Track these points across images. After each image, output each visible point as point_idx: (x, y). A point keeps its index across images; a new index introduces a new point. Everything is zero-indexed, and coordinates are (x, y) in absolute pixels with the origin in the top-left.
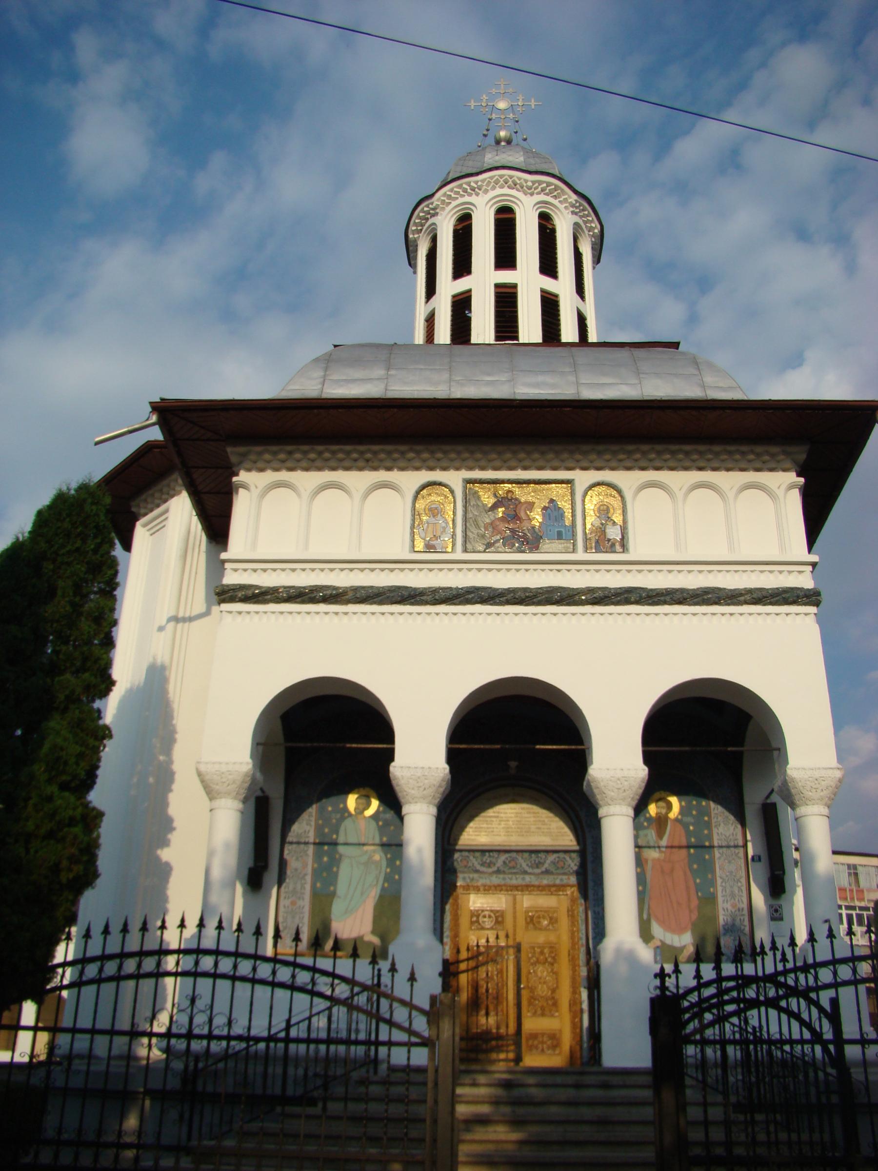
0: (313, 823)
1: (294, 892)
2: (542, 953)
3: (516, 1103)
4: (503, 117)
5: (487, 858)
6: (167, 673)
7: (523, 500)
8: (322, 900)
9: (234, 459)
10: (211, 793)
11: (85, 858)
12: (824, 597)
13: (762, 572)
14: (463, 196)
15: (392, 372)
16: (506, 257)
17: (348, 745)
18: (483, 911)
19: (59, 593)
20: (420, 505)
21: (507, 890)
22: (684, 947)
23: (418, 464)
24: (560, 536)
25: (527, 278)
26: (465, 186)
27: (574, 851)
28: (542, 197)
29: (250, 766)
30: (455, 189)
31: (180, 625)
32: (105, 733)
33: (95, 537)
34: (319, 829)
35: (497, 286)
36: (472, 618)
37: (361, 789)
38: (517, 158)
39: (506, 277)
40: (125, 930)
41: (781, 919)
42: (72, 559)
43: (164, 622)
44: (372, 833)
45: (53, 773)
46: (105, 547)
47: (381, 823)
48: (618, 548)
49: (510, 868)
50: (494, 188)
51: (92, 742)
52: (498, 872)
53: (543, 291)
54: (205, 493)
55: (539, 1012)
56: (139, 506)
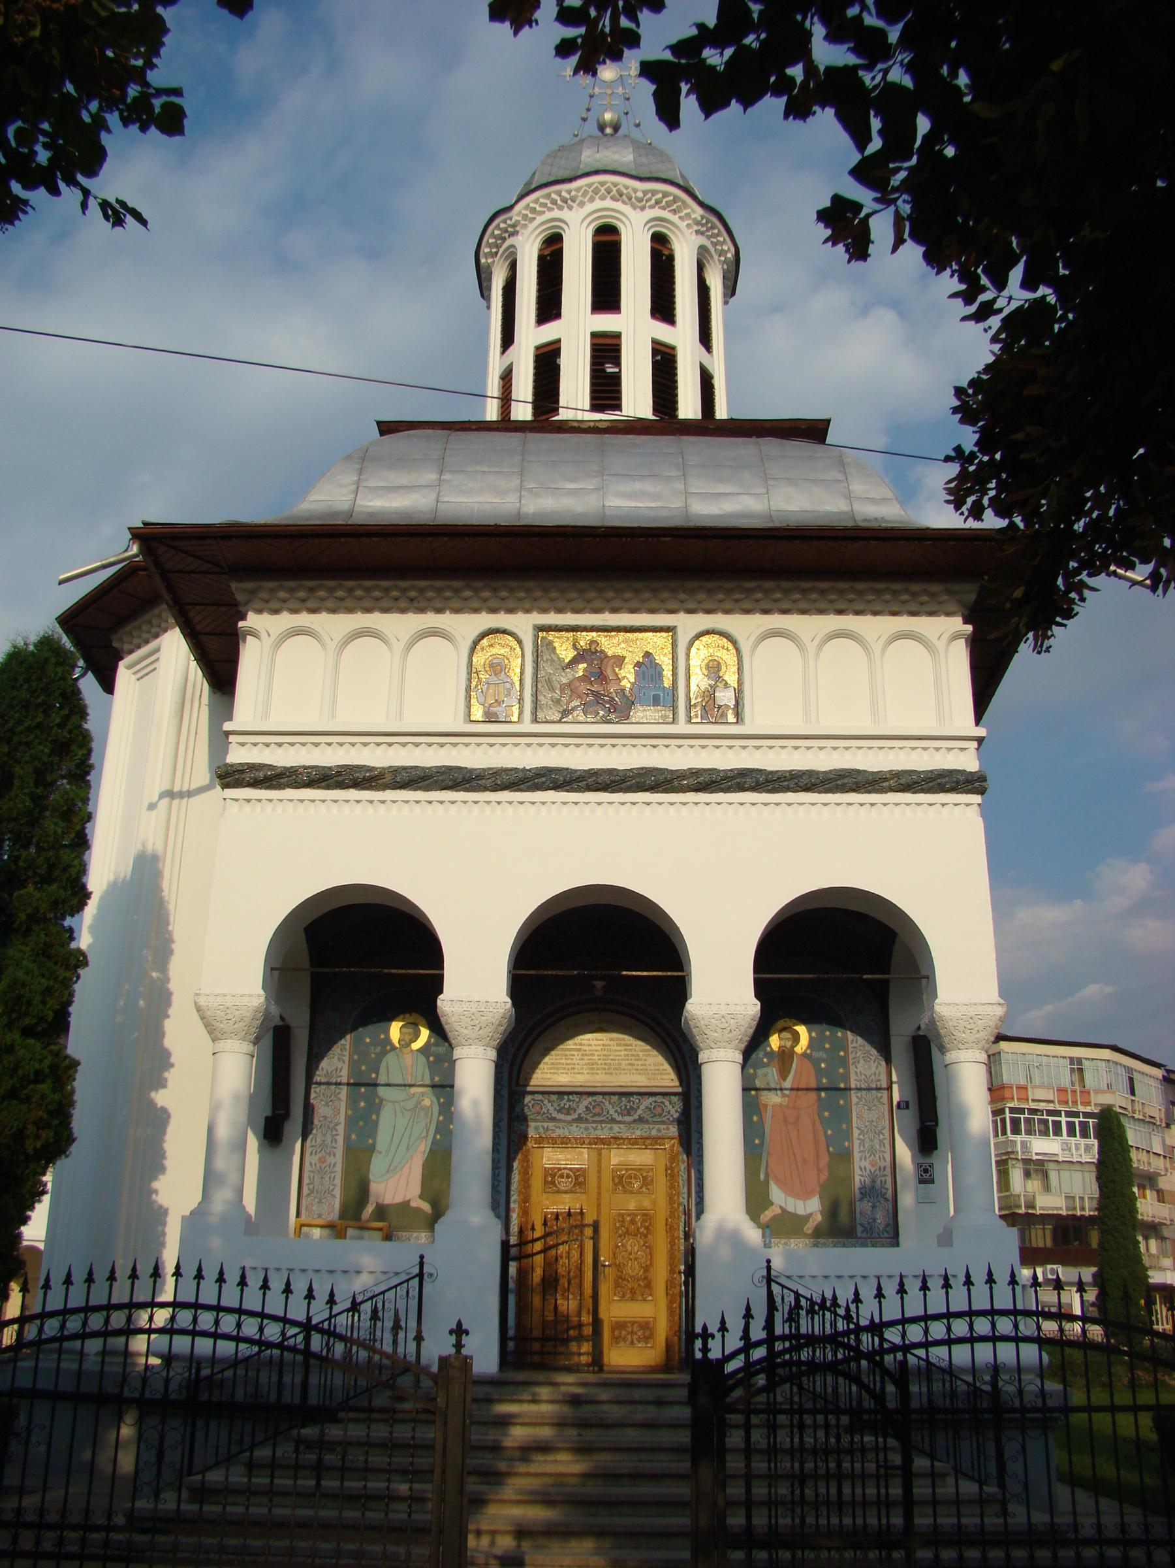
0: (346, 1059)
1: (323, 1145)
2: (633, 1222)
3: (583, 1424)
4: (609, 92)
5: (565, 1102)
6: (161, 865)
7: (610, 653)
8: (358, 1157)
9: (240, 597)
10: (214, 1033)
11: (56, 1122)
12: (990, 784)
13: (913, 749)
14: (551, 210)
15: (447, 477)
16: (606, 296)
17: (386, 971)
18: (560, 1169)
19: (17, 782)
20: (479, 659)
21: (590, 1144)
22: (811, 1214)
23: (476, 605)
24: (656, 701)
25: (635, 324)
26: (553, 196)
27: (675, 1094)
28: (657, 212)
29: (262, 999)
30: (542, 200)
31: (176, 802)
32: (79, 960)
33: (62, 707)
34: (353, 1066)
35: (594, 335)
36: (544, 808)
37: (407, 1015)
38: (624, 157)
39: (606, 322)
40: (90, 1279)
41: (932, 1181)
42: (32, 737)
43: (156, 798)
44: (420, 1071)
45: (14, 1016)
46: (75, 719)
47: (431, 1059)
48: (731, 718)
49: (595, 1115)
50: (592, 200)
51: (62, 973)
52: (579, 1120)
53: (655, 342)
54: (205, 634)
55: (628, 1296)
56: (121, 640)
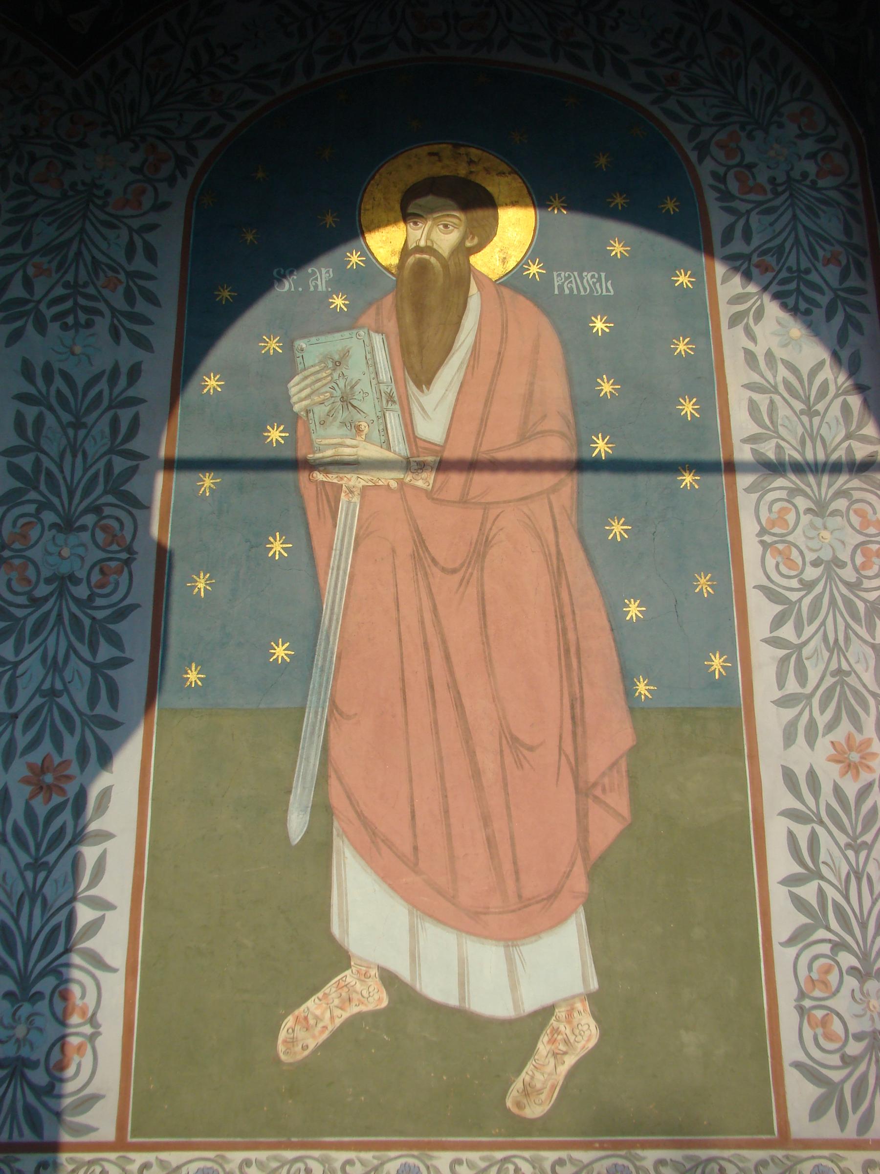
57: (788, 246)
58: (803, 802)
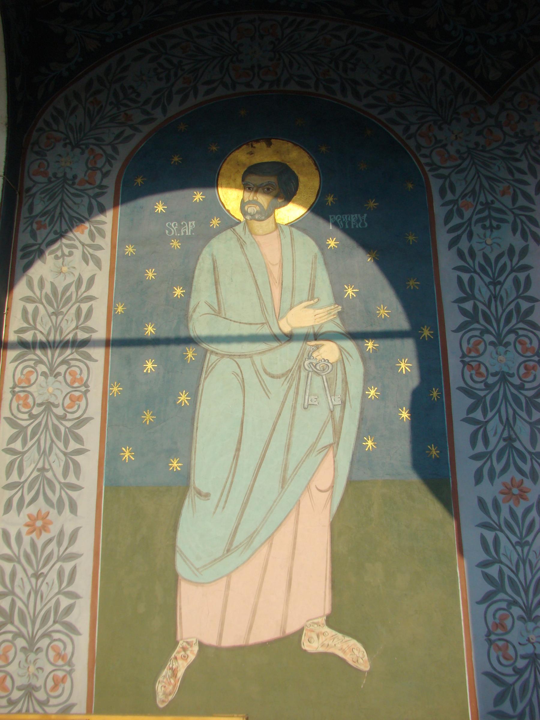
0: (105, 256)
57: (477, 188)
58: (490, 517)
